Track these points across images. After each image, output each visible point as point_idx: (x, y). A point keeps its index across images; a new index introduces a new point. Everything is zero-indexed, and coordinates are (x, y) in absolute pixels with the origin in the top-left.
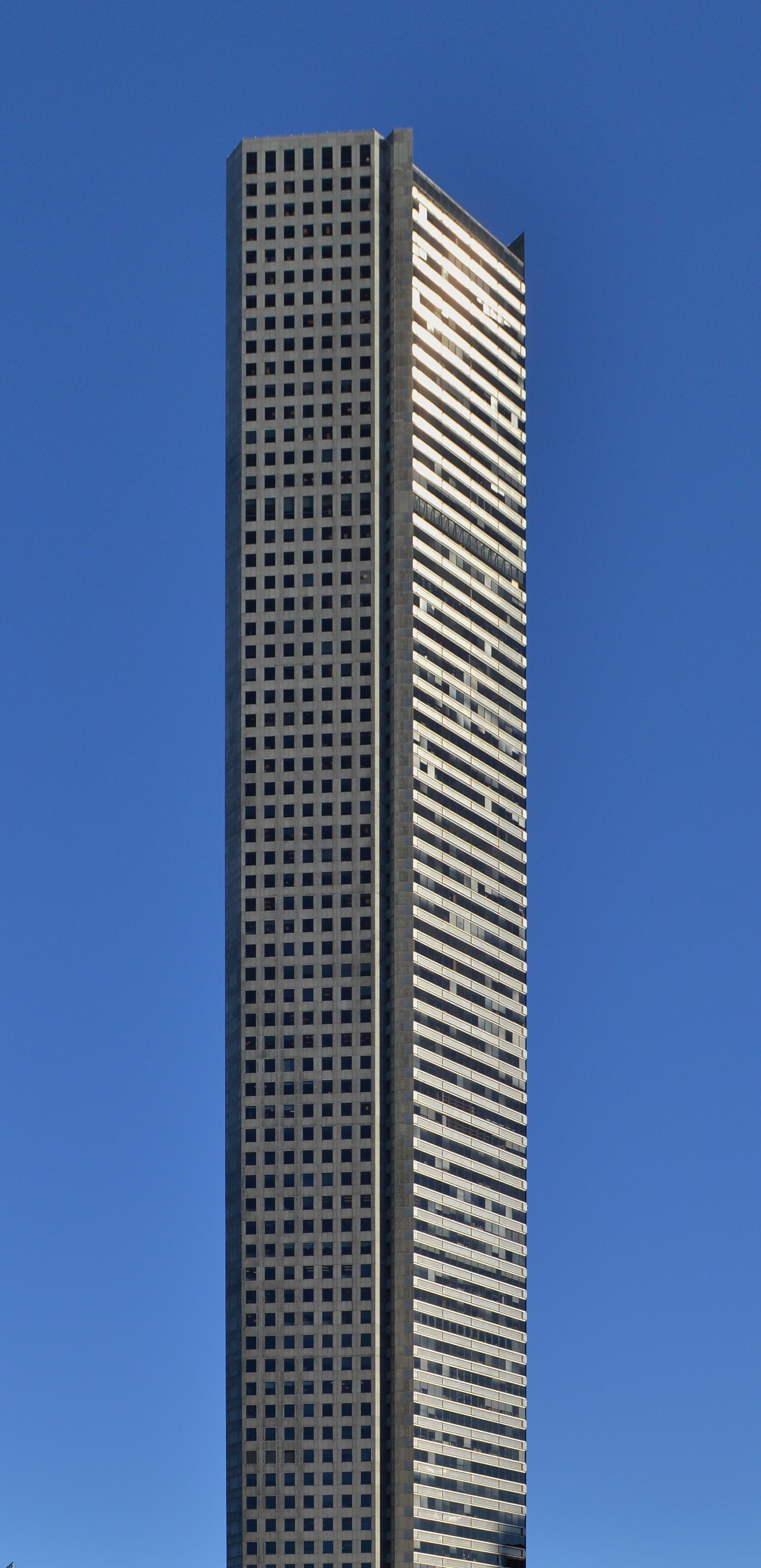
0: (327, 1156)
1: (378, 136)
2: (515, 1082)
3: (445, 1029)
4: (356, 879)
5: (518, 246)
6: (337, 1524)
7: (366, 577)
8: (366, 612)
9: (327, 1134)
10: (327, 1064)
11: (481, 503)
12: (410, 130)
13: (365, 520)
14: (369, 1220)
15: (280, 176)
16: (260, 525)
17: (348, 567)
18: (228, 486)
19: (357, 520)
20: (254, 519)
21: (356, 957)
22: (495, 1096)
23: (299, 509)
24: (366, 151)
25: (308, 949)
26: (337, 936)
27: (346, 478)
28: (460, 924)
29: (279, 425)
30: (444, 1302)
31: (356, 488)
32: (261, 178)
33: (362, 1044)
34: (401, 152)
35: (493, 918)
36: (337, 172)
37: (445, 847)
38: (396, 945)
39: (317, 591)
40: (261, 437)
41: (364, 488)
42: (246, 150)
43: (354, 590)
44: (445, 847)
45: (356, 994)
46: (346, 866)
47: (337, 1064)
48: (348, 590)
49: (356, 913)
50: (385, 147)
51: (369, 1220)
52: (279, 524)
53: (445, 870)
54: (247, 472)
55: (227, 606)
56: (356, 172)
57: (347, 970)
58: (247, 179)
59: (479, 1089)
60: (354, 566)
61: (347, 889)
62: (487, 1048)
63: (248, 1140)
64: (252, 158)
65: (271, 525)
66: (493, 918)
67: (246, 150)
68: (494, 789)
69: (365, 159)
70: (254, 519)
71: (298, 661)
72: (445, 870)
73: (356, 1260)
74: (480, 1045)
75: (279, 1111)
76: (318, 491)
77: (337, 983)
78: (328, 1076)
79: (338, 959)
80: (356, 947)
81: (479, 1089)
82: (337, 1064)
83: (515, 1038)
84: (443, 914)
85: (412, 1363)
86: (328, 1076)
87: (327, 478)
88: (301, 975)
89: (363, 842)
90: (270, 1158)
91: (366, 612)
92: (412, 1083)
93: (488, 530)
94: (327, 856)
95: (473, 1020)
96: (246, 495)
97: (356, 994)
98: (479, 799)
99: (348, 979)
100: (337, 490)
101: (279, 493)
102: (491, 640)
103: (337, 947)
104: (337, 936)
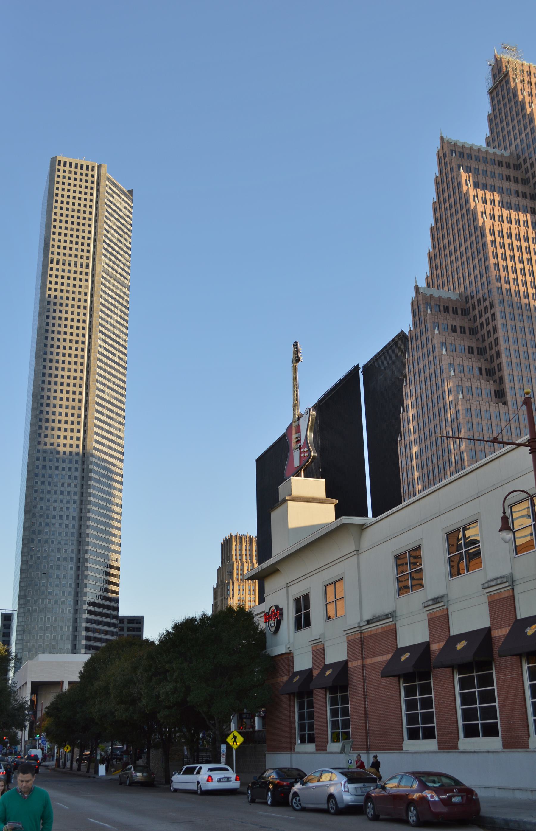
0: (67, 415)
1: (97, 164)
2: (121, 445)
3: (102, 429)
4: (78, 379)
5: (131, 192)
6: (75, 327)
7: (86, 287)
8: (79, 419)
9: (68, 385)
10: (65, 438)
11: (119, 266)
12: (106, 165)
13: (87, 270)
14: (81, 407)
15: (67, 168)
16: (54, 266)
17: (81, 283)
18: (44, 251)
19: (84, 270)
20: (53, 264)
21: (76, 404)
22: (115, 450)
23: (67, 264)
24: (93, 167)
25: (68, 285)
26: (71, 396)
27: (82, 257)
28: (108, 394)
29: (62, 238)
30: (93, 622)
31: (85, 261)
32: (62, 167)
33: (77, 432)
34: (103, 170)
35: (117, 392)
36: (84, 171)
37: (105, 371)
38: (89, 416)
39: (71, 289)
40: (57, 240)
41: (87, 261)
42: (58, 159)
43: (82, 290)
44: (105, 371)
45: (76, 416)
46: (75, 374)
47: (68, 438)
48: (80, 290)
49: (77, 389)
50: (99, 167)
51: (81, 407)
52: (60, 267)
53: (105, 378)
54: (51, 249)
55: (41, 286)
56: (90, 173)
57: (73, 408)
58: (58, 167)
59: (111, 448)
60: (83, 283)
61: (75, 381)
62: (114, 434)
63: (54, 221)
64: (59, 162)
65: (58, 266)
66: (117, 392)
67: (58, 159)
68: (119, 351)
69: (93, 170)
70: (53, 264)
71: (65, 281)
72: (105, 378)
73: (85, 261)
74: (111, 433)
75: (58, 297)
76: (73, 259)
77: (70, 411)
78: (65, 441)
79: (71, 403)
80: (77, 400)
81: (111, 448)
82: (68, 438)
83: (121, 430)
84: (103, 392)
85: (87, 511)
86: (65, 441)
87: (76, 256)
88: (58, 407)
89: (81, 360)
90: (59, 247)
91: (79, 419)
92: (93, 447)
93: (120, 274)
94: (69, 370)
95: (110, 425)
96: (51, 256)
97: (76, 416)
98: (114, 355)
99: (74, 410)
100: (79, 260)
101: (61, 257)
102: (120, 306)
103: (71, 400)
104: (71, 396)
